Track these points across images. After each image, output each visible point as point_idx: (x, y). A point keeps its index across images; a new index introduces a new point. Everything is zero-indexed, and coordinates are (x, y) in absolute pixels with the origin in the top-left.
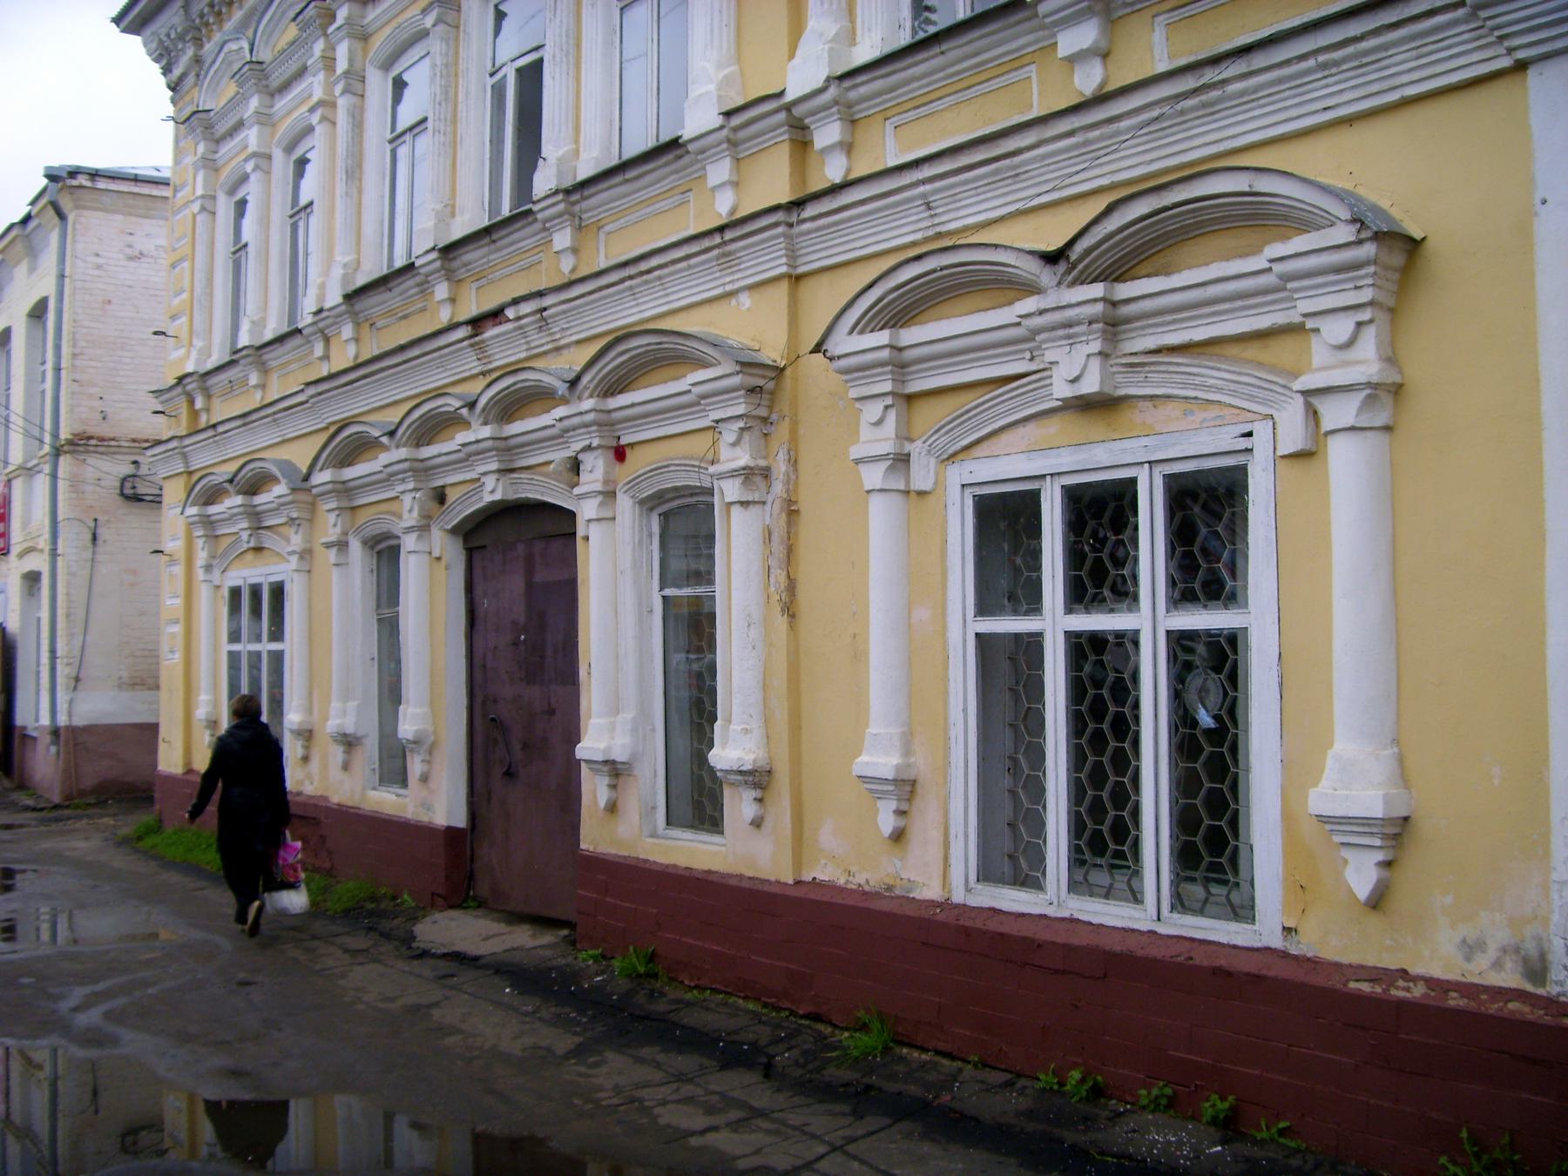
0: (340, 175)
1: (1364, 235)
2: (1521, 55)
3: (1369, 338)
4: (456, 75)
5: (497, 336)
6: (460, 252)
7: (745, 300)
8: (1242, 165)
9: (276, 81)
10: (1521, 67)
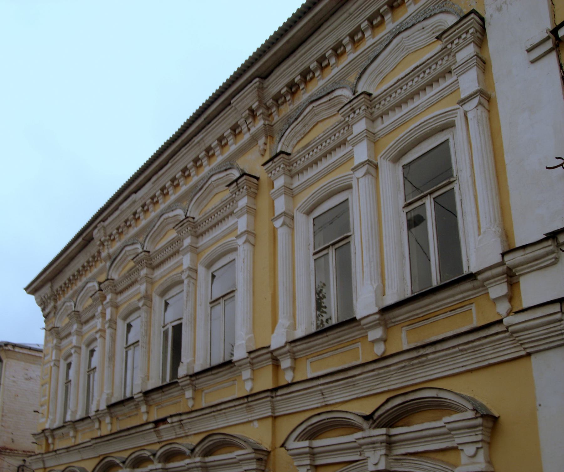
0: (107, 359)
1: (478, 415)
2: (529, 351)
3: (481, 453)
4: (150, 326)
5: (164, 429)
7: (256, 424)
9: (84, 319)
10: (529, 355)
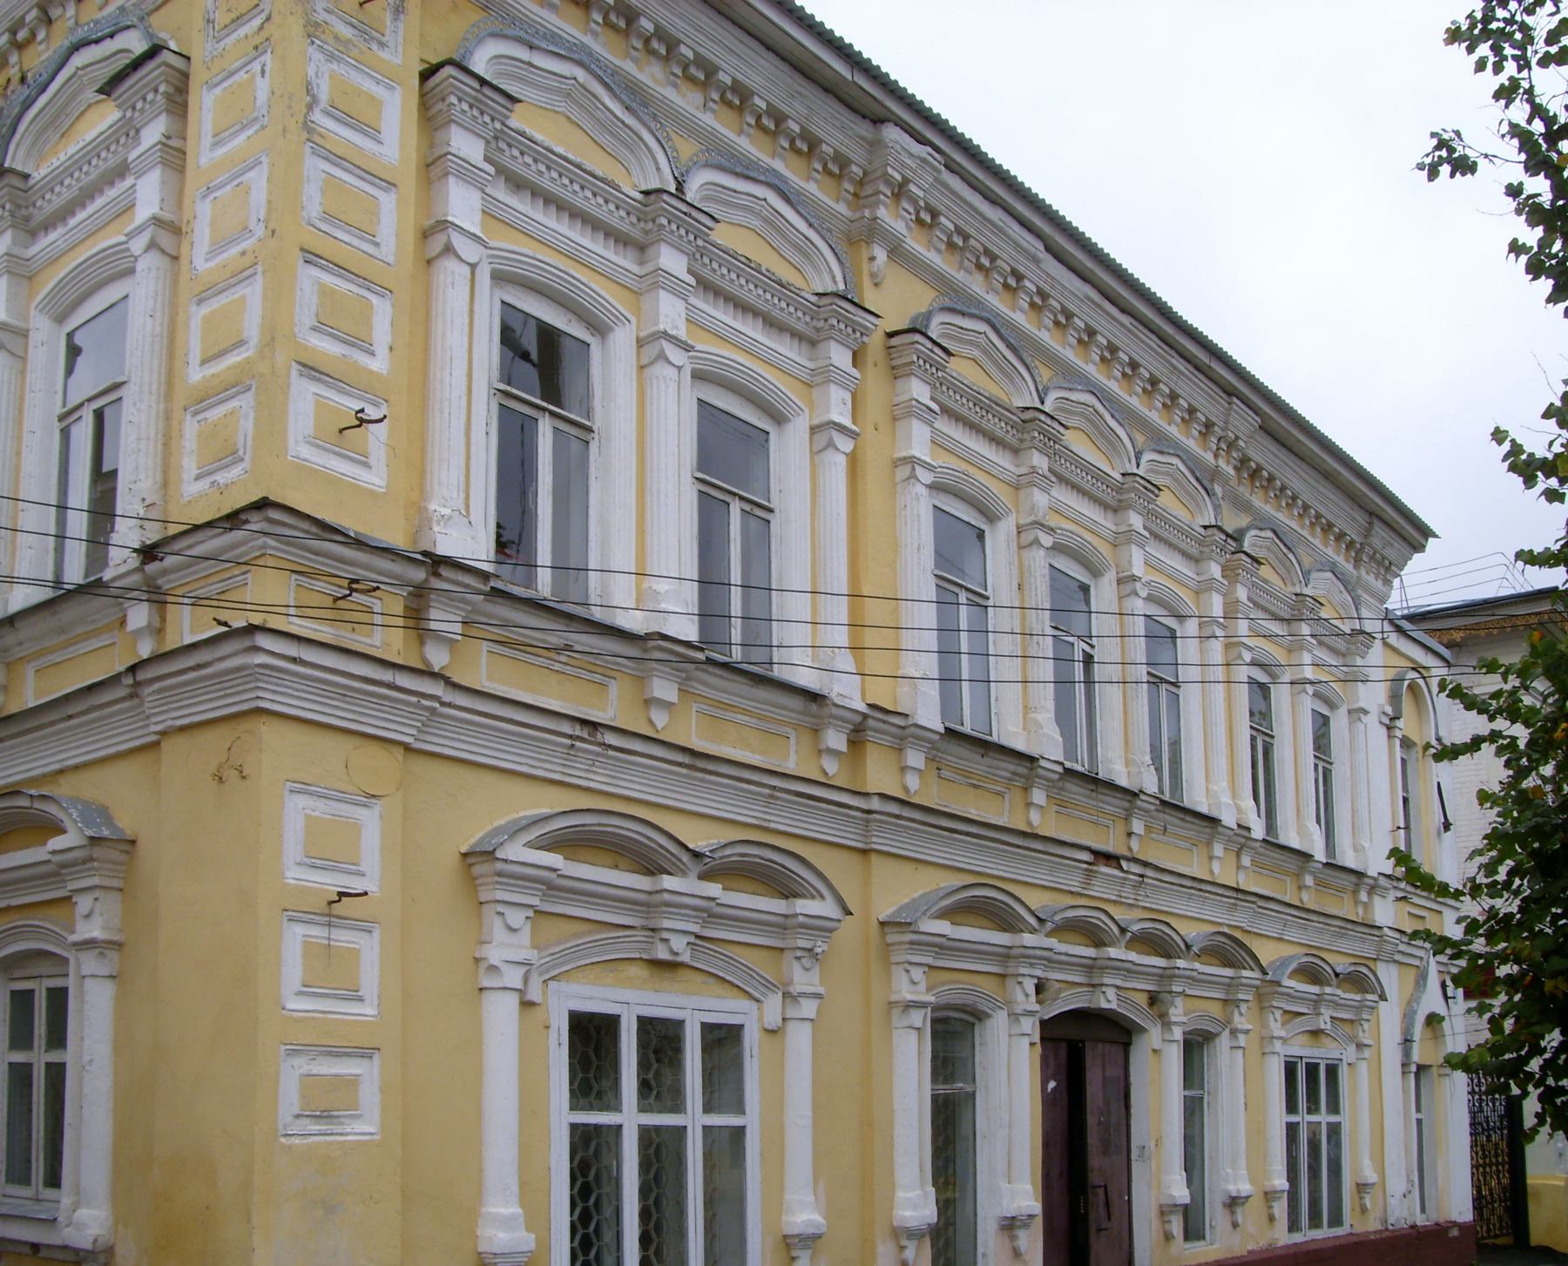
6: (1071, 780)
8: (1013, 892)
